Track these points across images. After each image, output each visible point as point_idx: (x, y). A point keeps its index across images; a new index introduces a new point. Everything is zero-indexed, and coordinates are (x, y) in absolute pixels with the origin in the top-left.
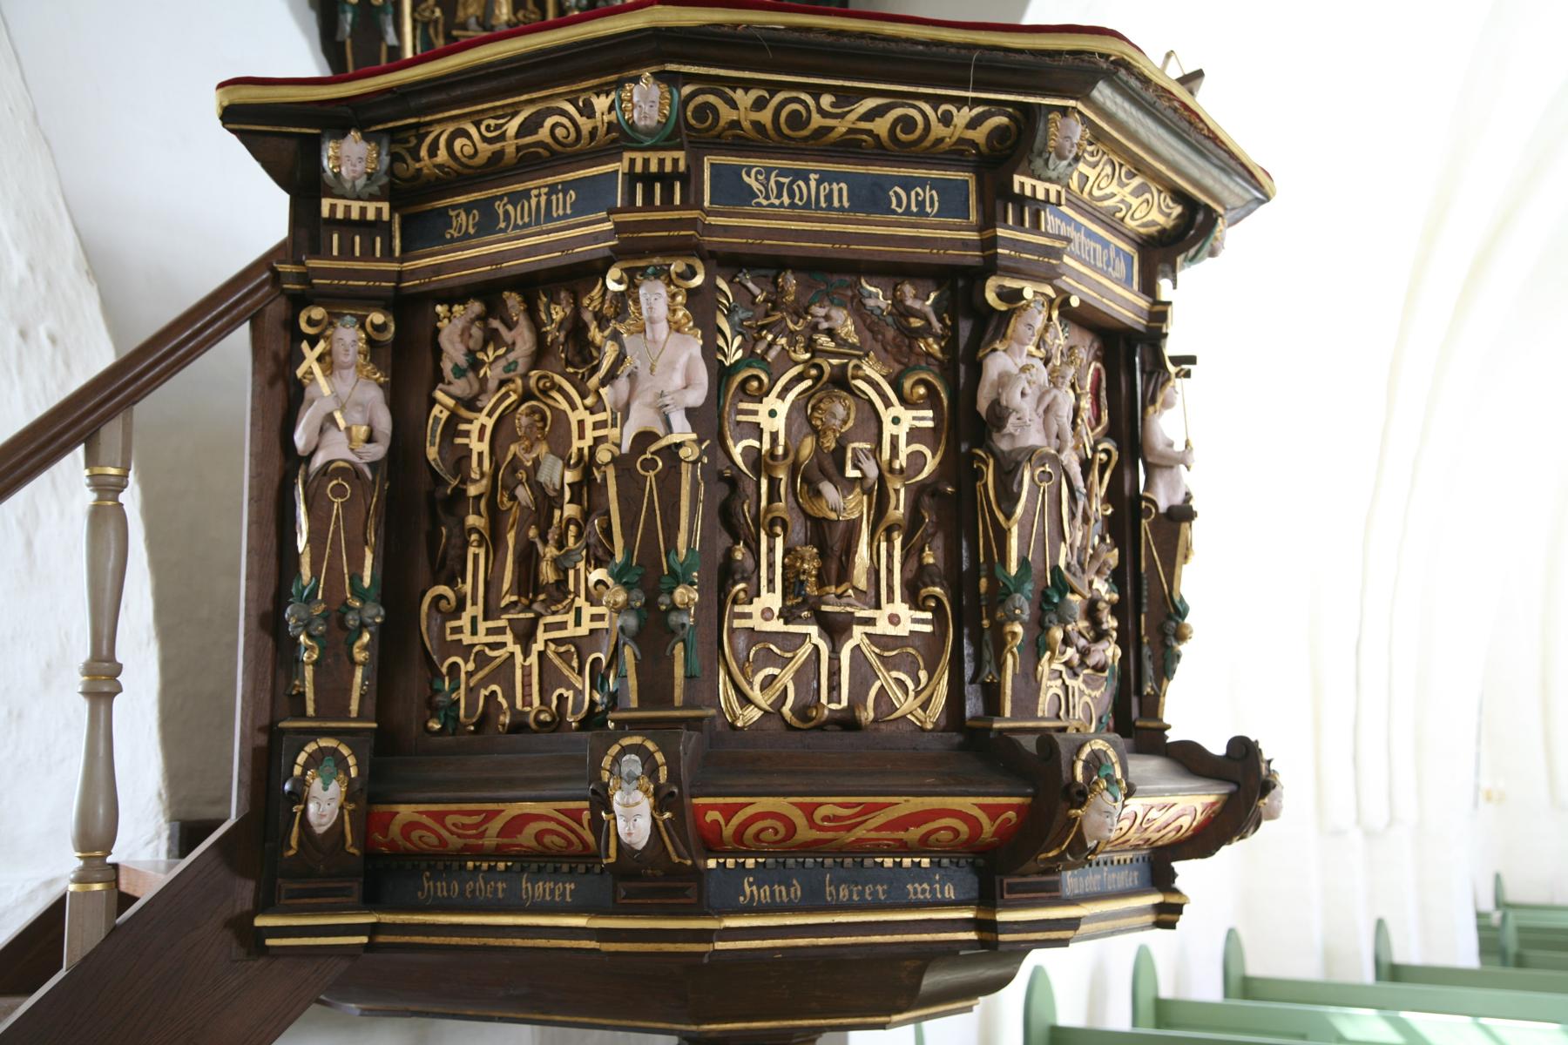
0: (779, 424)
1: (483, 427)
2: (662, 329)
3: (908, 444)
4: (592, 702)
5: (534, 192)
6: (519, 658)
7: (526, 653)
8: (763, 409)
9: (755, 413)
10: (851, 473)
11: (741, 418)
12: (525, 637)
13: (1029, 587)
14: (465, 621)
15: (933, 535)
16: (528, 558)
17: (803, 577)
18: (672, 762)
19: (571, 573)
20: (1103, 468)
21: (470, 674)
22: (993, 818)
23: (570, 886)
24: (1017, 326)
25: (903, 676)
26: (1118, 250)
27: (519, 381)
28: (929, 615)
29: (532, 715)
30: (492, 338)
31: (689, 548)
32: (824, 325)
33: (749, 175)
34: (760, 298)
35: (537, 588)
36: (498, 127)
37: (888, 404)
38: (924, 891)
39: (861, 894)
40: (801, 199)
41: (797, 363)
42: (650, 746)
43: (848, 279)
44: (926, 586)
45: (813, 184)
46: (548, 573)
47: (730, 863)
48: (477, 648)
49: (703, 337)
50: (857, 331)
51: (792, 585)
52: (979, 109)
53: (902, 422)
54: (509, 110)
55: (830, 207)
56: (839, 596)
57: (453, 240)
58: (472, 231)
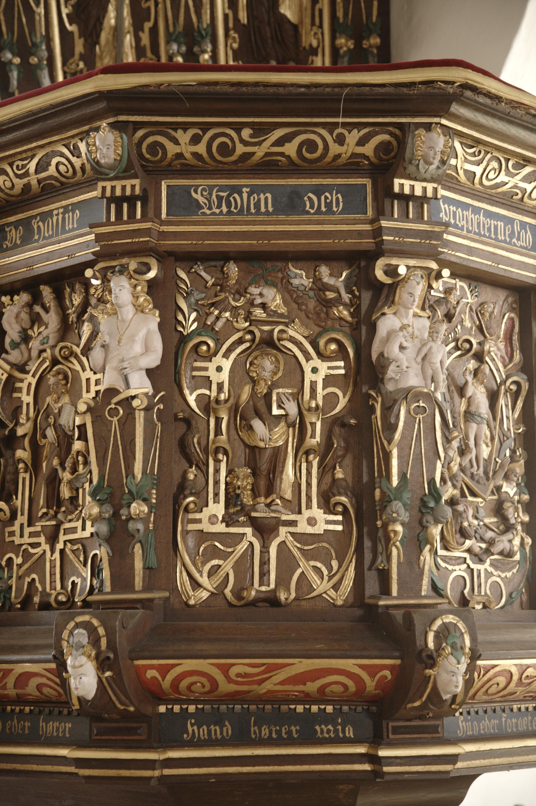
0: (225, 376)
1: (30, 384)
2: (128, 312)
3: (324, 388)
4: (91, 585)
5: (55, 212)
6: (48, 553)
7: (53, 551)
8: (212, 366)
9: (206, 369)
10: (276, 411)
11: (195, 373)
12: (53, 540)
13: (406, 496)
14: (16, 528)
15: (344, 456)
16: (54, 481)
17: (238, 492)
18: (110, 634)
19: (81, 491)
20: (516, 396)
21: (20, 566)
22: (372, 675)
23: (69, 725)
24: (401, 294)
25: (319, 565)
26: (523, 225)
27: (49, 351)
28: (340, 518)
29: (53, 597)
30: (35, 320)
31: (144, 472)
32: (258, 301)
33: (196, 192)
34: (210, 283)
35: (59, 503)
36: (24, 166)
37: (308, 358)
38: (329, 731)
39: (279, 733)
40: (236, 208)
41: (238, 330)
42: (95, 622)
43: (280, 264)
44: (334, 495)
45: (245, 196)
46: (65, 493)
47: (177, 708)
48: (24, 547)
49: (160, 316)
50: (285, 302)
51: (232, 499)
52: (366, 130)
53: (319, 371)
54: (30, 154)
55: (258, 212)
56: (268, 505)
57: (8, 249)
58: (18, 242)
